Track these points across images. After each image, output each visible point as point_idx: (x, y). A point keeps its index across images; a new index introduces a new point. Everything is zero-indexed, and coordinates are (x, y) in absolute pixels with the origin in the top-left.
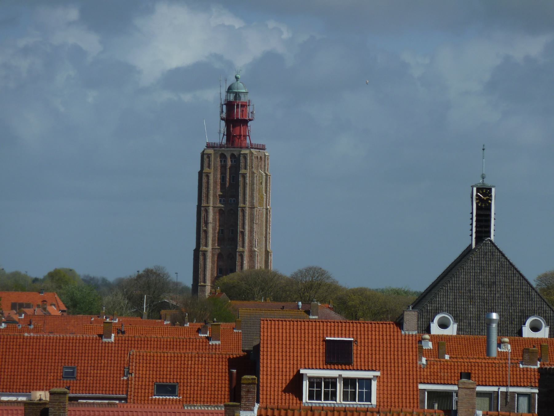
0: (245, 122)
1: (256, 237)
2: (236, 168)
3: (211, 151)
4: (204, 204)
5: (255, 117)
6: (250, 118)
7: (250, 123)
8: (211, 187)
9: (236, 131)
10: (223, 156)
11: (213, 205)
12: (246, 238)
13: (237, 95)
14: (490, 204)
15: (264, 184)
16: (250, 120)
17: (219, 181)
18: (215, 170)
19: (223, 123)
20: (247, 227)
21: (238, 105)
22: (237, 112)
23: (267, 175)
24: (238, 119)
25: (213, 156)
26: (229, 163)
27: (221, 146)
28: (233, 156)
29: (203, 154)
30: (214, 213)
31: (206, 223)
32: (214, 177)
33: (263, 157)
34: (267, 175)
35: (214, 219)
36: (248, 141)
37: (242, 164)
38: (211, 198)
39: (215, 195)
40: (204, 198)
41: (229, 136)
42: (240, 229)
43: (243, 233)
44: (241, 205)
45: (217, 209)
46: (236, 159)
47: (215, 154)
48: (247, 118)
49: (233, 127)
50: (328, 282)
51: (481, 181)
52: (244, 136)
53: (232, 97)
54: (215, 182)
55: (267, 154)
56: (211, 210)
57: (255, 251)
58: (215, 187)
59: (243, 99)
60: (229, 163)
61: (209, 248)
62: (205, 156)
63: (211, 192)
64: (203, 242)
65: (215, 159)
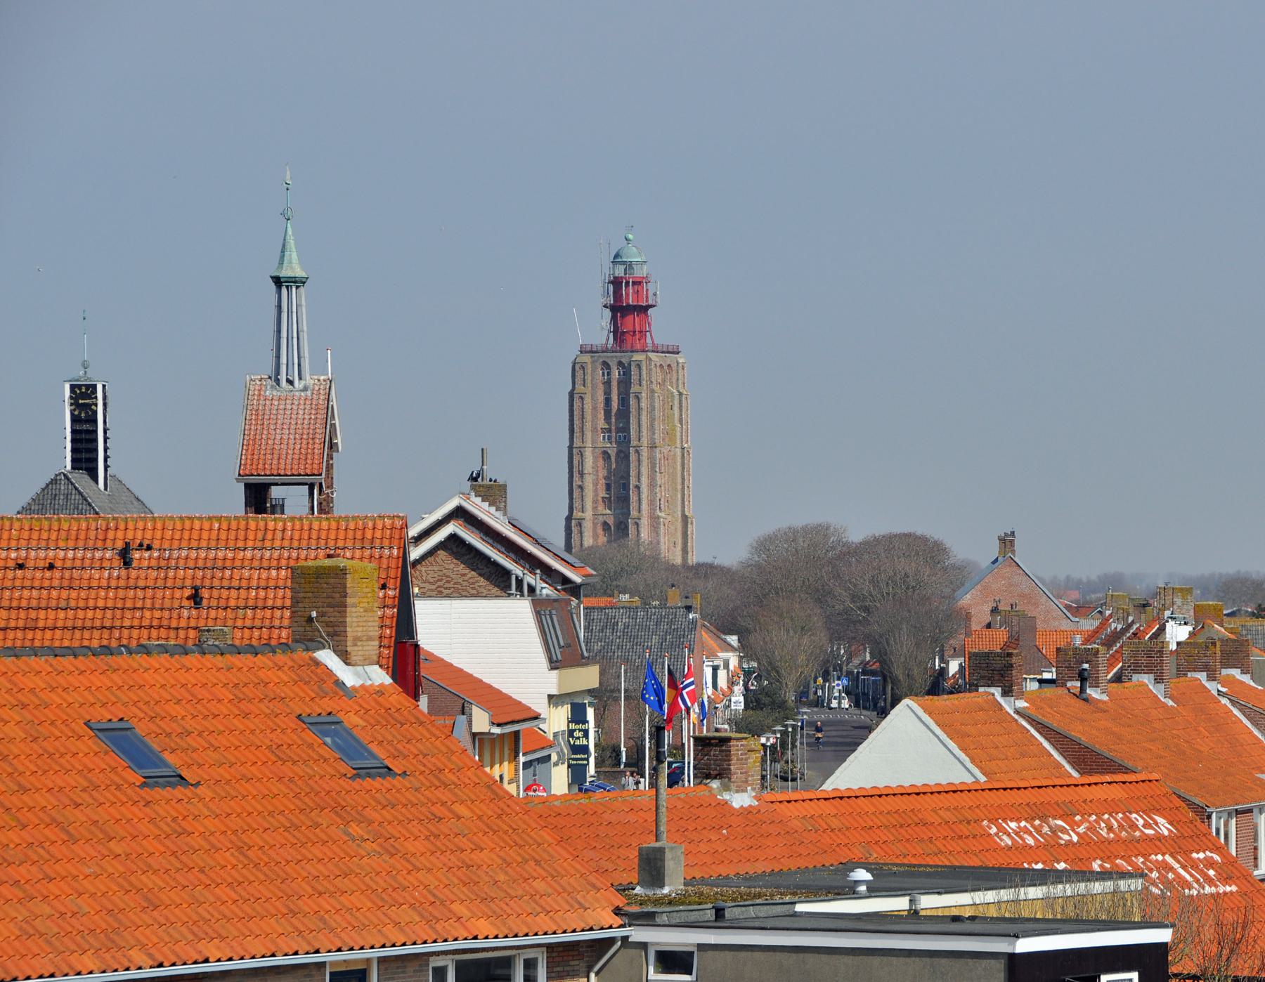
0: (644, 309)
1: (661, 493)
2: (625, 383)
3: (586, 358)
4: (577, 443)
5: (659, 300)
6: (650, 302)
7: (650, 311)
8: (588, 417)
9: (630, 322)
10: (606, 365)
11: (594, 442)
12: (644, 496)
13: (629, 266)
14: (95, 413)
15: (676, 408)
16: (651, 306)
17: (601, 406)
18: (594, 387)
19: (608, 313)
20: (644, 480)
21: (627, 283)
22: (627, 294)
23: (681, 394)
24: (628, 305)
25: (590, 366)
26: (615, 374)
27: (605, 350)
28: (620, 363)
29: (574, 364)
30: (595, 458)
31: (582, 474)
32: (593, 401)
33: (674, 366)
34: (681, 394)
35: (595, 468)
36: (649, 340)
37: (634, 378)
38: (588, 435)
39: (594, 430)
40: (577, 434)
41: (618, 334)
42: (633, 481)
43: (638, 487)
44: (634, 443)
45: (598, 451)
46: (626, 369)
47: (593, 362)
48: (644, 304)
49: (622, 317)
50: (511, 555)
51: (82, 373)
52: (641, 332)
53: (620, 271)
54: (595, 408)
55: (681, 361)
56: (588, 453)
57: (659, 517)
58: (595, 416)
59: (639, 272)
60: (615, 374)
61: (589, 514)
62: (577, 367)
63: (588, 425)
64: (577, 504)
65: (594, 371)
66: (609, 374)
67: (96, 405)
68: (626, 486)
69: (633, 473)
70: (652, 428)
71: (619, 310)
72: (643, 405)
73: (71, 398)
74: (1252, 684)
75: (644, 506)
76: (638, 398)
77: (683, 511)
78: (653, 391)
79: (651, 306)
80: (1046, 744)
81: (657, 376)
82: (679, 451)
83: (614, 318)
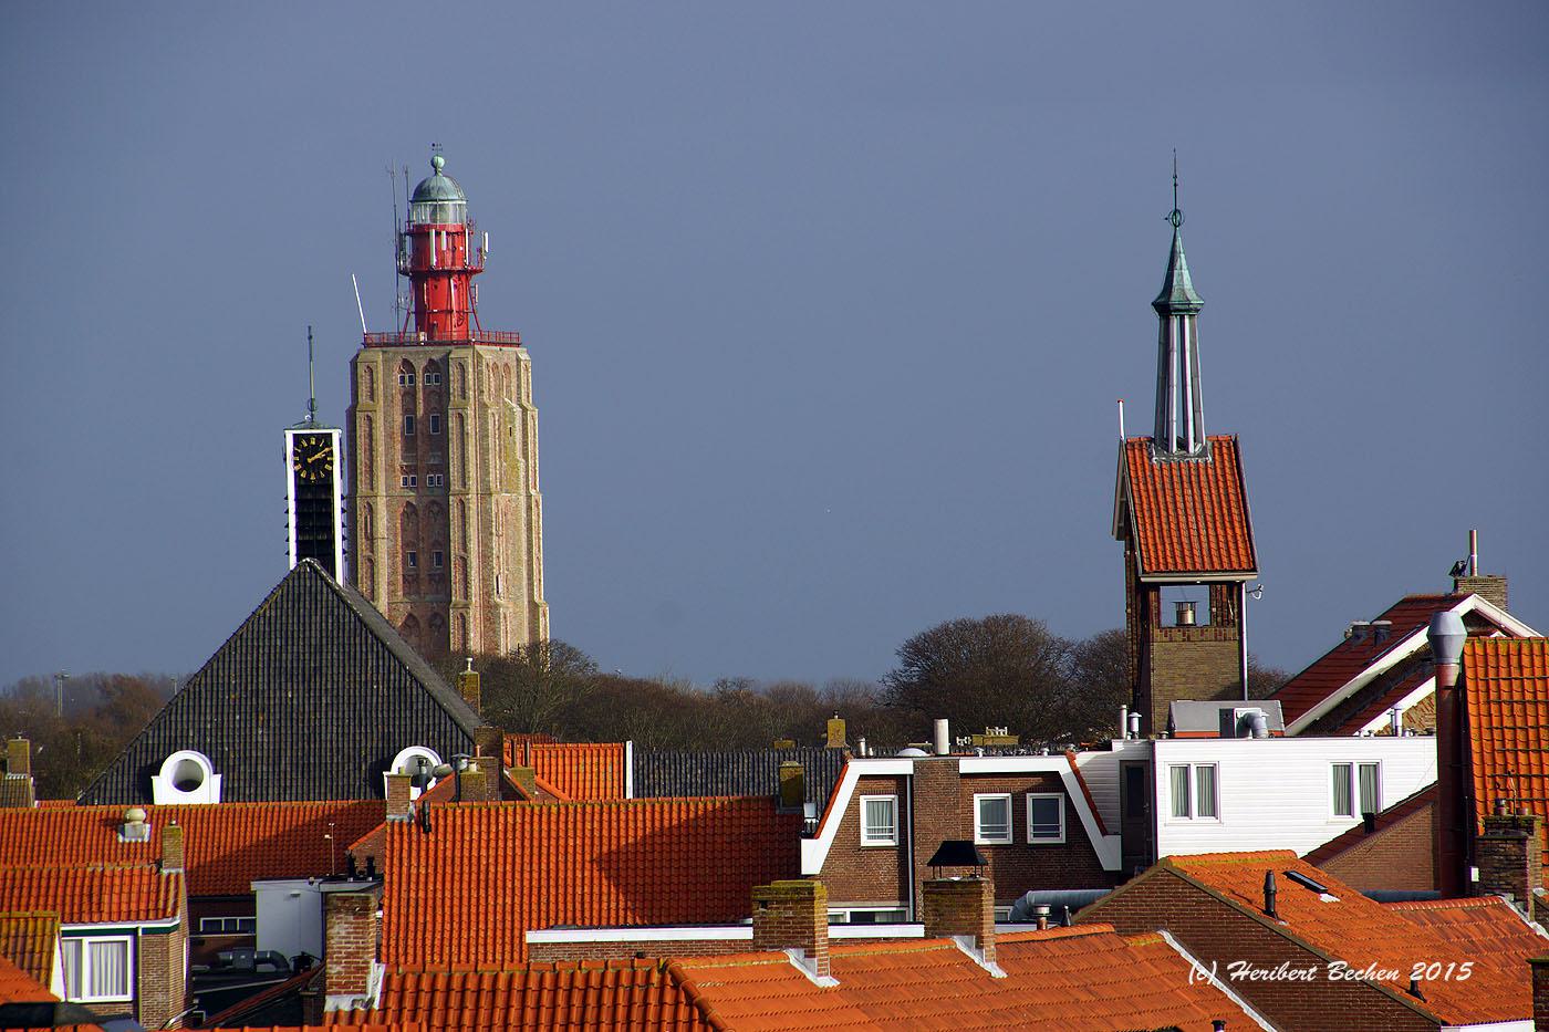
1: (500, 568)
16: (475, 272)
19: (405, 281)
31: (371, 538)
40: (362, 478)
43: (465, 561)
53: (423, 215)
57: (497, 606)
63: (381, 461)
66: (411, 380)
67: (331, 463)
68: (443, 558)
69: (455, 535)
70: (484, 466)
71: (421, 274)
72: (470, 428)
73: (295, 453)
74: (340, 804)
75: (475, 588)
76: (462, 418)
77: (531, 595)
78: (484, 406)
79: (475, 272)
80: (1247, 1009)
81: (490, 382)
82: (523, 499)
83: (418, 290)
